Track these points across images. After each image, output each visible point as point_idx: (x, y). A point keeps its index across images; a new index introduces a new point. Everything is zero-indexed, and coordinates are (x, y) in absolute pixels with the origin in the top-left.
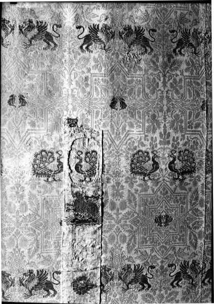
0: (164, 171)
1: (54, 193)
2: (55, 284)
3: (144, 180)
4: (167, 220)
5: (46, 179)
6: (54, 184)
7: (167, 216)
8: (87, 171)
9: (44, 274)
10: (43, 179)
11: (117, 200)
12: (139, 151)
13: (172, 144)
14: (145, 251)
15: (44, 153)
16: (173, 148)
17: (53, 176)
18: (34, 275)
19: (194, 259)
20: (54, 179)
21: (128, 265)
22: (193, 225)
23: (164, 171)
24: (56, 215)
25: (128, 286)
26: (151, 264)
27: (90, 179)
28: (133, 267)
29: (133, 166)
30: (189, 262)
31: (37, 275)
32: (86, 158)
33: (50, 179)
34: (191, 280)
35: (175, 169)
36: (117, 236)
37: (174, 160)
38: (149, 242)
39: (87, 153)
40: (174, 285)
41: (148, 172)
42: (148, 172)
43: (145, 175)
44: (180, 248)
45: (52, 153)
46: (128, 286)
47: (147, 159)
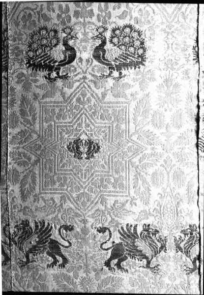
0: (84, 63)
1: (58, 97)
2: (63, 246)
3: (48, 78)
4: (90, 148)
5: (46, 73)
6: (59, 83)
7: (90, 143)
8: (114, 61)
9: (47, 228)
10: (43, 73)
11: (166, 110)
12: (41, 29)
13: (98, 15)
14: (52, 199)
15: (128, 30)
16: (101, 24)
17: (58, 69)
18: (31, 228)
19: (147, 222)
20: (58, 73)
21: (190, 226)
22: (140, 161)
23: (84, 63)
24: (61, 133)
25: (27, 257)
26: (63, 223)
27: (120, 73)
28: (32, 225)
29: (141, 51)
30: (136, 226)
31: (36, 230)
32: (112, 37)
33: (54, 74)
34: (145, 261)
35: (105, 60)
36: (168, 174)
37: (104, 43)
38: (57, 184)
39: (114, 31)
40: (112, 266)
41: (57, 64)
42: (57, 64)
43: (50, 69)
44: (116, 202)
45: (56, 32)
46: (27, 257)
47: (54, 42)
